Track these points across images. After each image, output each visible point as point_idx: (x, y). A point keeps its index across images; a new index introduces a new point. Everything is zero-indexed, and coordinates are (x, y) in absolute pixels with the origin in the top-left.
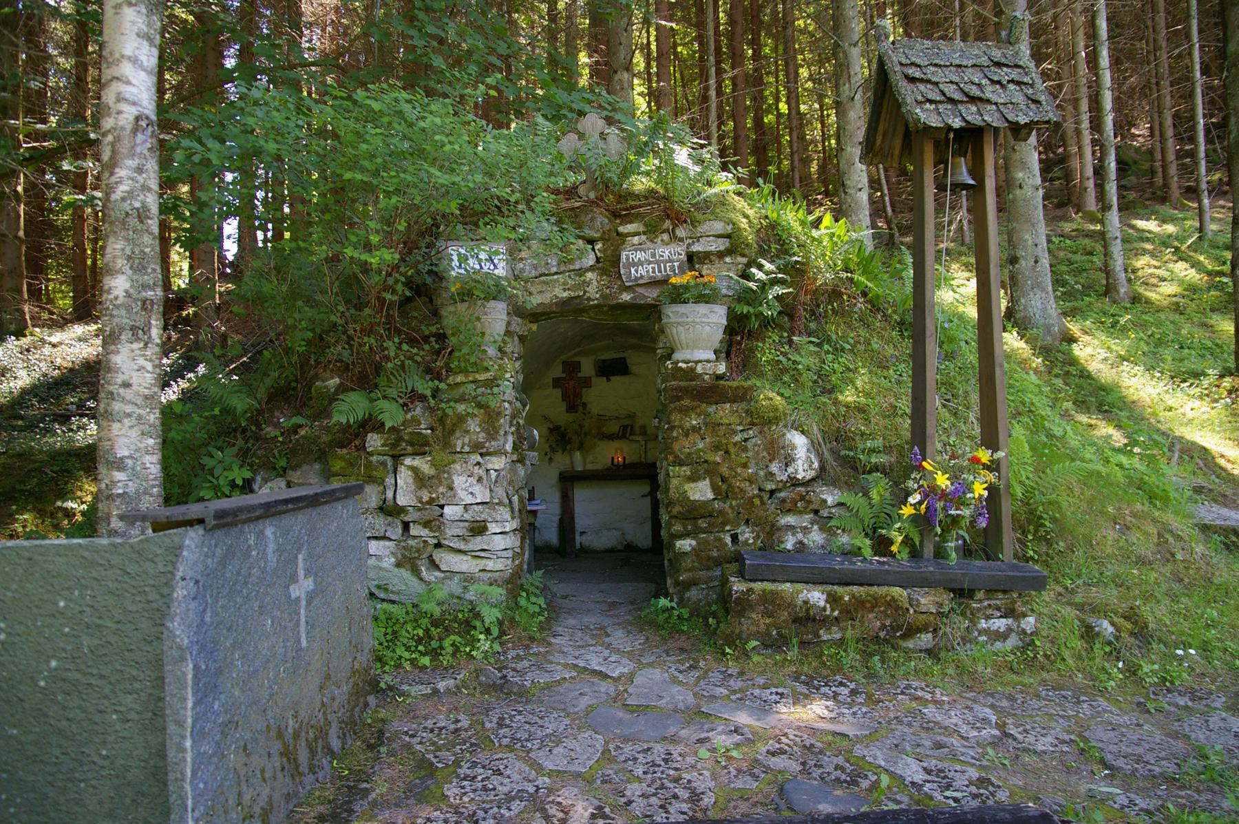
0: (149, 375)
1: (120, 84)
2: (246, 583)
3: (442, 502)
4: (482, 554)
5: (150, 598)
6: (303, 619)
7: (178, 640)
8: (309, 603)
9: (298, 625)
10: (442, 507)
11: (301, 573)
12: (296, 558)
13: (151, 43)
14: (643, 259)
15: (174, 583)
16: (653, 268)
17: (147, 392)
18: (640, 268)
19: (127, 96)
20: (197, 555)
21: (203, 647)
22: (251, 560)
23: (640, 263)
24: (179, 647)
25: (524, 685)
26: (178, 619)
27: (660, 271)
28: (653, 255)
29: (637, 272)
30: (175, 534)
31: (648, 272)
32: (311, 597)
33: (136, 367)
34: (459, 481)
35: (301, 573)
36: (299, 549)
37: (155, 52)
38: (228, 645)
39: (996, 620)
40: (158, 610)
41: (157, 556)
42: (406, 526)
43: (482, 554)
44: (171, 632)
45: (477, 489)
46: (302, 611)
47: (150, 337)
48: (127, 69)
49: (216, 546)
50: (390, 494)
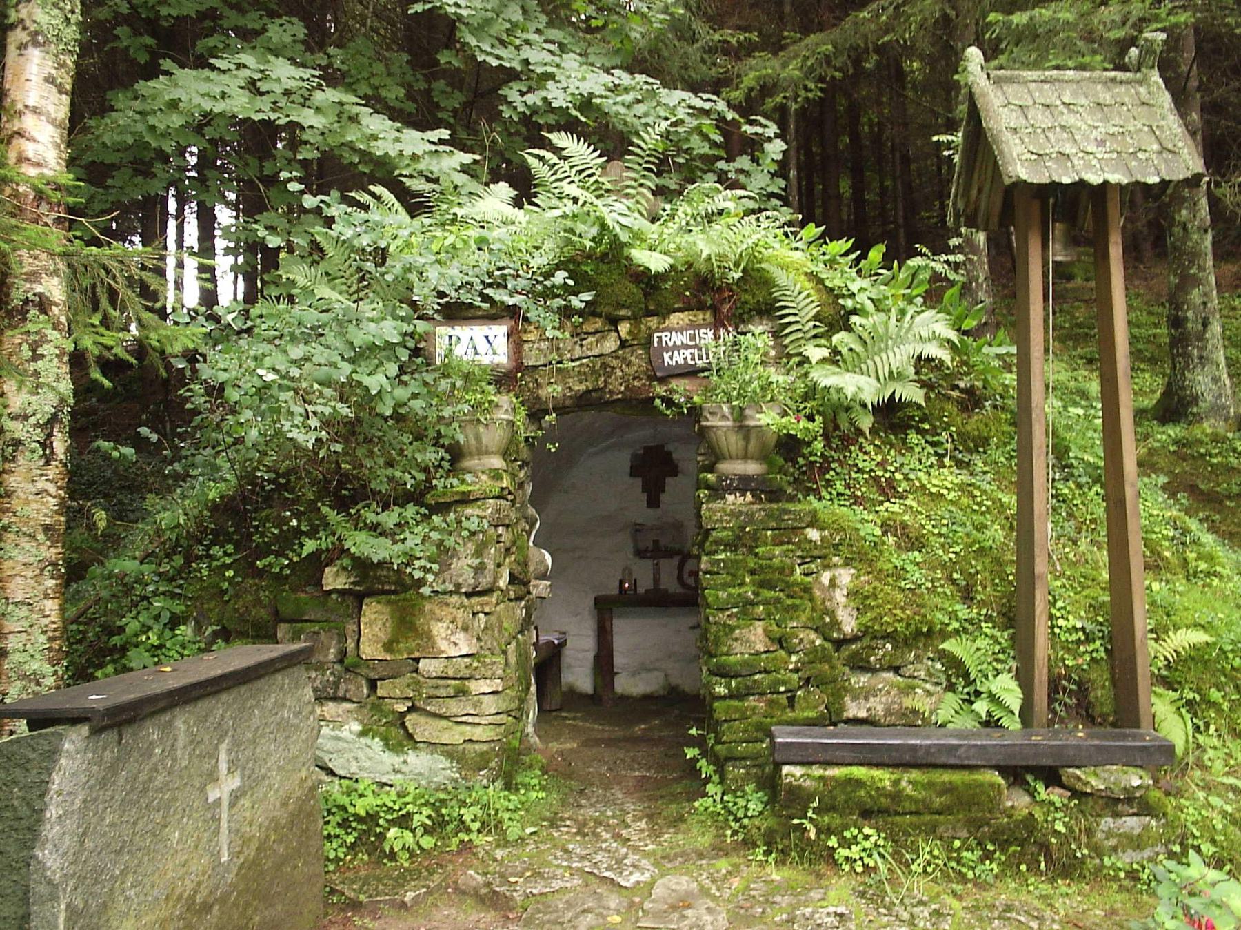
0: (50, 499)
1: (22, 141)
2: (145, 790)
3: (417, 655)
4: (470, 719)
5: (20, 814)
6: (224, 824)
7: (49, 873)
8: (232, 805)
9: (217, 832)
10: (417, 660)
11: (223, 766)
12: (216, 748)
13: (61, 91)
14: (679, 343)
15: (47, 799)
16: (693, 354)
17: (48, 521)
18: (676, 353)
19: (30, 155)
20: (78, 762)
21: (81, 879)
22: (154, 760)
23: (675, 347)
24: (50, 882)
25: (512, 898)
26: (49, 846)
27: (701, 358)
28: (693, 338)
29: (671, 358)
30: (53, 733)
31: (685, 359)
32: (235, 797)
33: (34, 490)
34: (439, 630)
35: (223, 766)
36: (221, 740)
37: (66, 99)
38: (117, 872)
39: (1128, 819)
40: (28, 829)
41: (29, 761)
42: (373, 685)
43: (470, 719)
44: (39, 862)
45: (460, 637)
46: (224, 816)
47: (52, 453)
48: (29, 123)
49: (105, 749)
50: (350, 645)
